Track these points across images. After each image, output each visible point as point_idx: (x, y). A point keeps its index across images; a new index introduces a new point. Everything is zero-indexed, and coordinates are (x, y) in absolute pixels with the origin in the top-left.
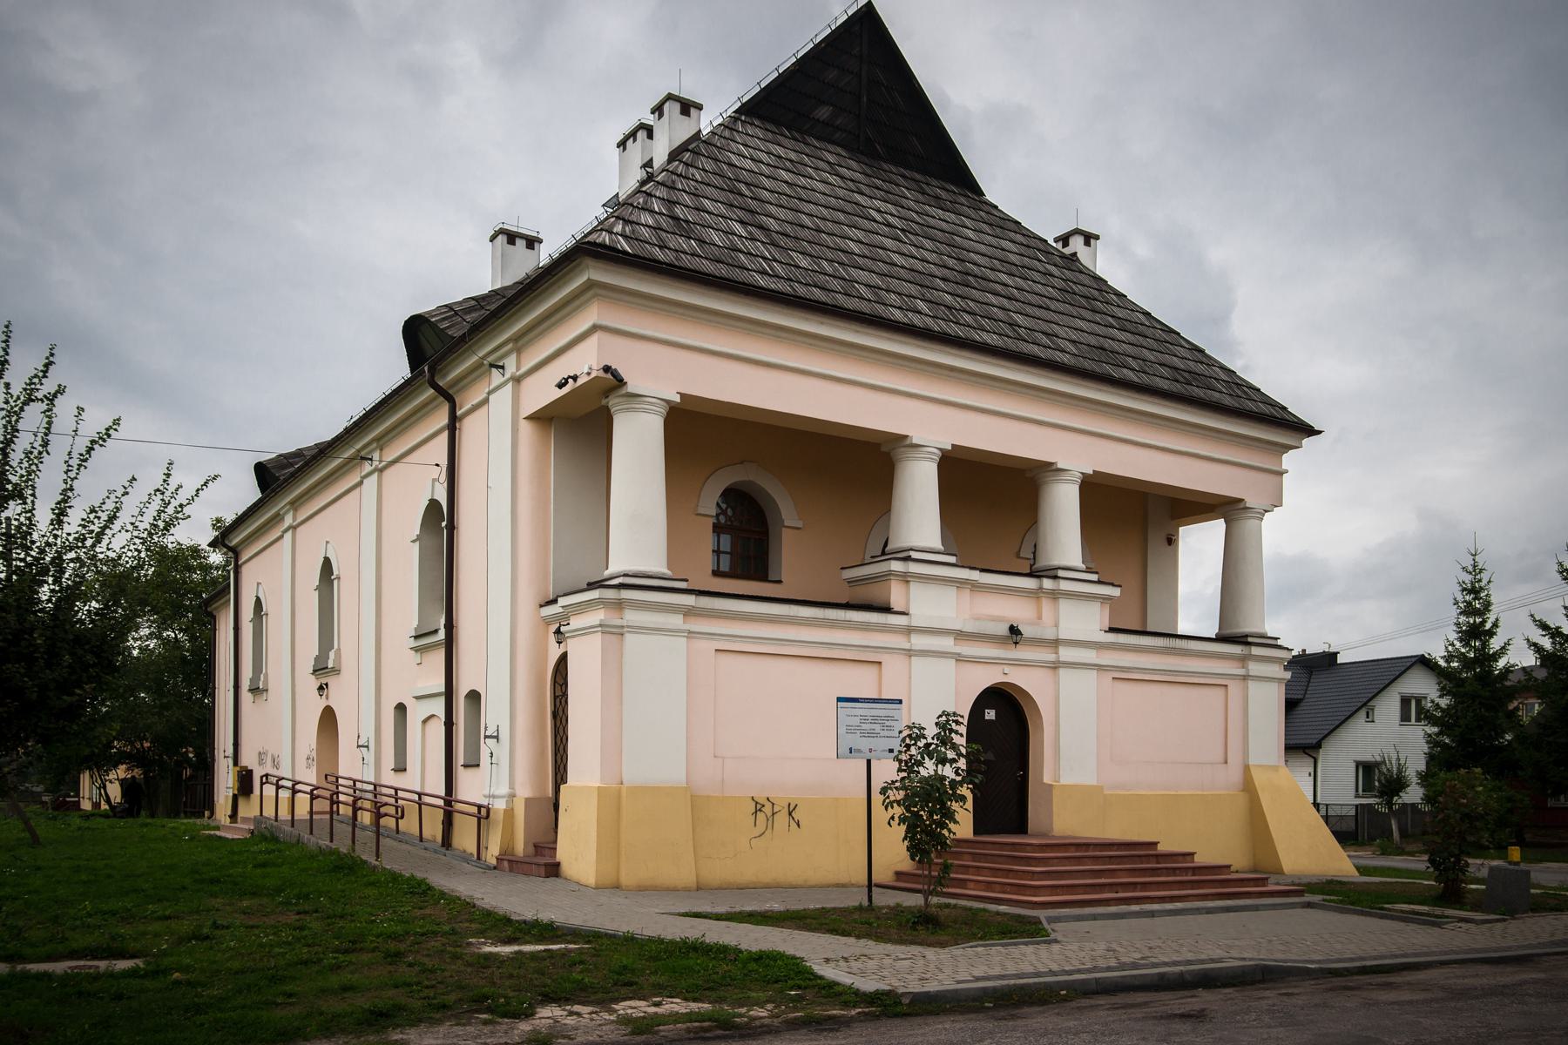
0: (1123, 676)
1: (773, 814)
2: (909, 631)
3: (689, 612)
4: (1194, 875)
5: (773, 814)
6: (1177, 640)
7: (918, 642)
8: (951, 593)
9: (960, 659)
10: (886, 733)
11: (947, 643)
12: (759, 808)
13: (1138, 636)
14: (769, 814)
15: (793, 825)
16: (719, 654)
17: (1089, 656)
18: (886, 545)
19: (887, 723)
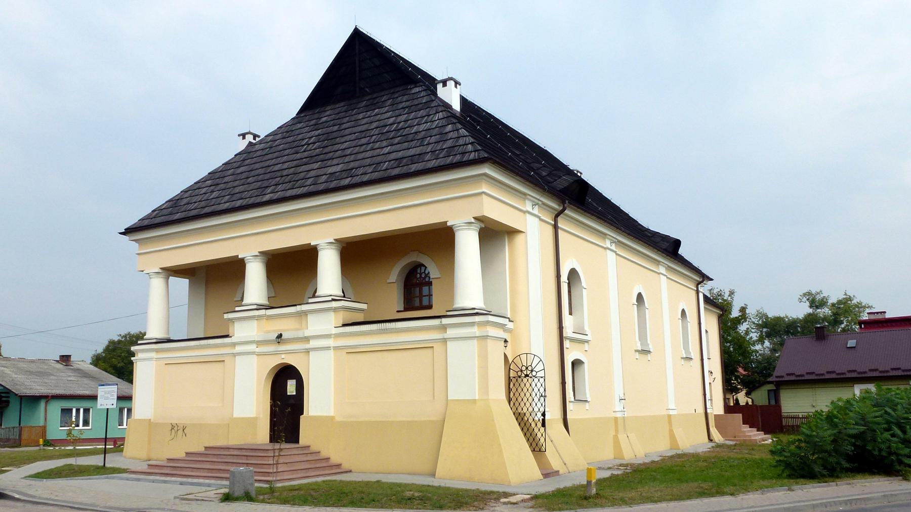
0: (353, 351)
1: (178, 430)
2: (234, 345)
3: (157, 351)
4: (247, 459)
5: (178, 430)
6: (387, 324)
7: (239, 349)
8: (254, 323)
9: (260, 354)
10: (112, 398)
11: (252, 348)
12: (173, 427)
13: (359, 326)
14: (176, 430)
15: (184, 435)
16: (167, 365)
17: (331, 342)
18: (315, 292)
19: (112, 393)
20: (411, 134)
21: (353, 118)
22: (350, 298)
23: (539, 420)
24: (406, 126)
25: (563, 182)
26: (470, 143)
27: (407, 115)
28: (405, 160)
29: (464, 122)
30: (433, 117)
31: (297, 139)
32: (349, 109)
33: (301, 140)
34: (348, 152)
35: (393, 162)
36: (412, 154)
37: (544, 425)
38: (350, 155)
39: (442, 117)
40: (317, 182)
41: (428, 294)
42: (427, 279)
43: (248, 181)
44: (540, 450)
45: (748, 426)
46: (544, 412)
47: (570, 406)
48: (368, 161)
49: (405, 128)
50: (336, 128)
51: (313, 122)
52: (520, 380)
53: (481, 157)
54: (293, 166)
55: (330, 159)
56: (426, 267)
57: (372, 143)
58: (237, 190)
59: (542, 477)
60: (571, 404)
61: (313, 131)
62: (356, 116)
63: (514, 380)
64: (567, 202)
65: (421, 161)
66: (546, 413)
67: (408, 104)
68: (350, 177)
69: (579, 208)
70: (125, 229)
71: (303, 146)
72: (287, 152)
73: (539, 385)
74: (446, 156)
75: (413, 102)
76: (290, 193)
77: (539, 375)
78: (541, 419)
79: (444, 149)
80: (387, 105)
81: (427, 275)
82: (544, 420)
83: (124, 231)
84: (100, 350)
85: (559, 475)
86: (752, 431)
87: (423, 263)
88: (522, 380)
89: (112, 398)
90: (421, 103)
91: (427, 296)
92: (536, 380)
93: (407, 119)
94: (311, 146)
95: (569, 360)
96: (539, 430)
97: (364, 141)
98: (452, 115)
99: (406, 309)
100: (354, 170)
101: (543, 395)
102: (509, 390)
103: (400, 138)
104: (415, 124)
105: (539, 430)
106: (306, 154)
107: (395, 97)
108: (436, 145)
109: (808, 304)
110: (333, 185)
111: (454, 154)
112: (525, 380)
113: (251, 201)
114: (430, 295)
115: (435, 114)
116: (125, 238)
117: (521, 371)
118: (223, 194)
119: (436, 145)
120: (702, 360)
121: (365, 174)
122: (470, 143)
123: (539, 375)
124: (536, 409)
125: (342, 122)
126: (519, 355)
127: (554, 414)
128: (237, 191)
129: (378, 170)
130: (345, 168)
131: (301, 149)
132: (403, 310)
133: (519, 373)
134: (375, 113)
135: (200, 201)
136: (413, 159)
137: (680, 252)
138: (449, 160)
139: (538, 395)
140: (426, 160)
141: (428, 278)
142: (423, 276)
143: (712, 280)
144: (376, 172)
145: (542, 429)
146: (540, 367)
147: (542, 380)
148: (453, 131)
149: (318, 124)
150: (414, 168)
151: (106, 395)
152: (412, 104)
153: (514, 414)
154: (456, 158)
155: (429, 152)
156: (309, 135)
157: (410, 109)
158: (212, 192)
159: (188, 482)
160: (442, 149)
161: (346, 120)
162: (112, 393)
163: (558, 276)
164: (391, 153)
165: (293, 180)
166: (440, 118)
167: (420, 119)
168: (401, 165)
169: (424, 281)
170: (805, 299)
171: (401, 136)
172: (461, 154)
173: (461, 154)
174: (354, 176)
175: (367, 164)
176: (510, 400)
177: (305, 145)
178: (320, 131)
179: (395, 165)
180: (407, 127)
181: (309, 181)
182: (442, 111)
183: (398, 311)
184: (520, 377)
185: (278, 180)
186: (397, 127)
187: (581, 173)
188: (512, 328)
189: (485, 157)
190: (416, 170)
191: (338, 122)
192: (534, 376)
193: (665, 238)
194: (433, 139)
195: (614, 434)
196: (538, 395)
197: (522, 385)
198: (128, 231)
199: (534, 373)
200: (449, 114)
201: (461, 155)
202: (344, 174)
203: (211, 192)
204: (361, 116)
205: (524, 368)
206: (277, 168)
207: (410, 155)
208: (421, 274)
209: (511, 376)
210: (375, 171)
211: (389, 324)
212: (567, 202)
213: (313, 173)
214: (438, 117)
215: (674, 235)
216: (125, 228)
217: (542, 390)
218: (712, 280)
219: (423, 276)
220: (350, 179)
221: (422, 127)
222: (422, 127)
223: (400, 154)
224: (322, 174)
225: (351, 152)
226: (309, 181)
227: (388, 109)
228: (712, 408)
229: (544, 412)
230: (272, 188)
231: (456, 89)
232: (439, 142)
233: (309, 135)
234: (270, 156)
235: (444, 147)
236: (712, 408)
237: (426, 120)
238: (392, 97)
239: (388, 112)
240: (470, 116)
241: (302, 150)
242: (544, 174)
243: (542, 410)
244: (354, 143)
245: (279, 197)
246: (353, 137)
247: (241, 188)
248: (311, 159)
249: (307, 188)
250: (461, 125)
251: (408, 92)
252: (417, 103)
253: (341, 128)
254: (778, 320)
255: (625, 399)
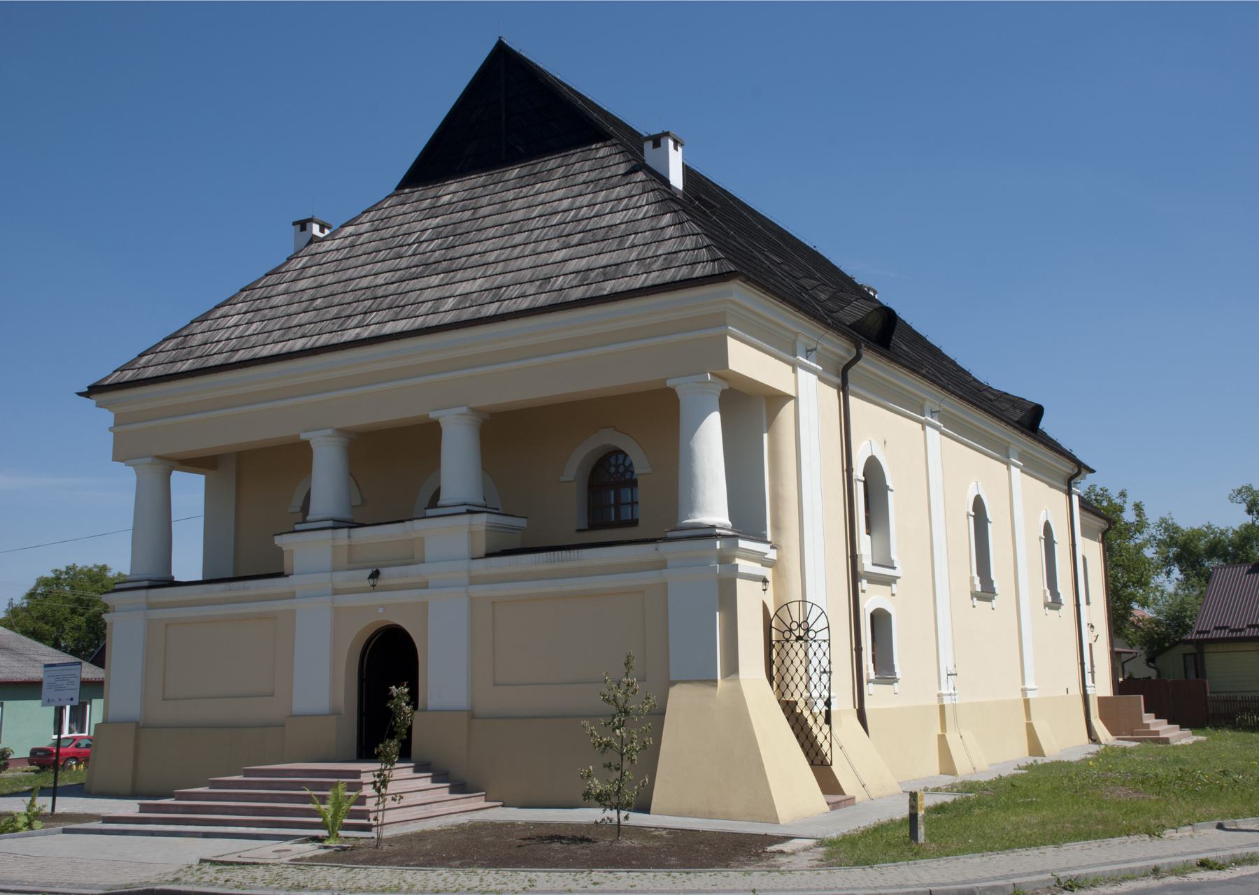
6: (564, 552)
18: (436, 495)
19: (71, 680)
20: (601, 228)
21: (496, 198)
22: (497, 509)
23: (820, 712)
24: (592, 214)
25: (854, 312)
26: (705, 247)
27: (592, 195)
28: (593, 274)
29: (690, 208)
30: (638, 200)
31: (398, 233)
32: (489, 182)
33: (405, 234)
34: (492, 257)
35: (571, 276)
36: (604, 263)
37: (828, 720)
38: (496, 262)
39: (653, 200)
40: (438, 309)
41: (630, 501)
42: (628, 476)
43: (314, 305)
44: (822, 762)
45: (1153, 715)
46: (829, 699)
47: (869, 689)
48: (527, 275)
49: (590, 218)
50: (468, 214)
51: (426, 203)
52: (787, 646)
53: (724, 271)
54: (394, 279)
55: (460, 270)
56: (626, 455)
57: (534, 242)
58: (296, 320)
59: (827, 808)
60: (871, 685)
61: (429, 218)
62: (503, 194)
63: (778, 646)
64: (863, 345)
65: (620, 276)
66: (832, 700)
67: (593, 175)
68: (498, 301)
69: (881, 354)
70: (88, 387)
71: (409, 245)
72: (382, 255)
73: (820, 654)
74: (663, 267)
75: (601, 172)
76: (389, 328)
77: (820, 636)
78: (823, 711)
79: (661, 255)
80: (556, 177)
81: (629, 468)
82: (828, 713)
83: (87, 390)
84: (19, 599)
85: (854, 804)
86: (1160, 724)
87: (623, 449)
88: (792, 646)
89: (72, 687)
90: (616, 176)
91: (629, 504)
92: (815, 645)
93: (593, 202)
94: (425, 244)
95: (867, 607)
96: (821, 729)
97: (519, 238)
98: (671, 197)
99: (593, 526)
100: (504, 288)
101: (827, 669)
102: (769, 663)
103: (582, 234)
104: (607, 211)
105: (821, 729)
106: (416, 259)
107: (570, 162)
108: (646, 248)
109: (1244, 506)
110: (466, 315)
111: (678, 264)
112: (796, 645)
113: (323, 340)
114: (634, 503)
115: (642, 194)
116: (90, 403)
117: (791, 630)
118: (269, 328)
119: (646, 248)
120: (1078, 605)
121: (523, 296)
122: (705, 247)
123: (820, 636)
124: (815, 694)
125: (478, 205)
126: (787, 604)
127: (843, 704)
128: (295, 323)
129: (547, 290)
130: (487, 286)
131: (407, 251)
132: (587, 527)
133: (787, 635)
134: (535, 190)
135: (227, 339)
136: (609, 271)
137: (1040, 427)
138: (669, 276)
139: (818, 671)
140: (629, 273)
141: (629, 473)
142: (621, 469)
143: (1092, 471)
144: (542, 293)
145: (826, 728)
146: (822, 623)
147: (824, 646)
148: (675, 225)
149: (435, 207)
150: (608, 287)
151: (58, 683)
152: (601, 176)
153: (779, 702)
154: (681, 272)
155: (633, 261)
156: (419, 226)
157: (597, 185)
158: (250, 323)
159: (1076, 869)
160: (657, 256)
161: (485, 200)
162: (71, 680)
163: (849, 470)
164: (567, 261)
165: (395, 305)
166: (650, 202)
167: (616, 202)
168: (585, 283)
169: (623, 479)
170: (1239, 499)
171: (583, 232)
172: (690, 264)
173: (690, 264)
174: (505, 300)
175: (526, 280)
176: (771, 679)
177: (413, 243)
178: (438, 219)
179: (574, 283)
180: (593, 217)
181: (424, 308)
182: (652, 191)
183: (579, 531)
184: (787, 640)
185: (369, 305)
186: (576, 215)
187: (875, 292)
188: (776, 559)
189: (731, 272)
190: (614, 291)
191: (472, 203)
192: (812, 639)
193: (1016, 402)
194: (639, 239)
195: (940, 733)
196: (818, 671)
197: (792, 654)
198: (95, 390)
199: (811, 634)
200: (666, 196)
201: (690, 266)
202: (487, 296)
203: (247, 323)
204: (511, 195)
205: (794, 626)
206: (365, 282)
207: (602, 266)
208: (617, 467)
209: (774, 638)
210: (540, 291)
211: (568, 552)
212: (863, 345)
213: (428, 294)
214: (647, 200)
215: (1033, 397)
216: (89, 384)
217: (825, 662)
218: (1092, 471)
219: (621, 469)
220: (497, 304)
221: (618, 218)
222: (618, 218)
223: (583, 263)
224: (447, 294)
225: (497, 257)
226: (424, 308)
227: (558, 185)
228: (1094, 687)
229: (829, 699)
230: (359, 317)
231: (675, 151)
232: (651, 243)
233: (419, 226)
234: (352, 262)
235: (658, 254)
236: (1094, 687)
237: (627, 205)
238: (565, 163)
239: (559, 189)
240: (698, 198)
241: (410, 252)
242: (823, 297)
243: (825, 694)
244: (500, 242)
245: (373, 335)
246: (501, 230)
247: (304, 318)
248: (428, 267)
249: (421, 319)
250: (688, 214)
251: (593, 154)
252: (609, 174)
253: (477, 216)
254: (1196, 535)
255: (956, 675)
